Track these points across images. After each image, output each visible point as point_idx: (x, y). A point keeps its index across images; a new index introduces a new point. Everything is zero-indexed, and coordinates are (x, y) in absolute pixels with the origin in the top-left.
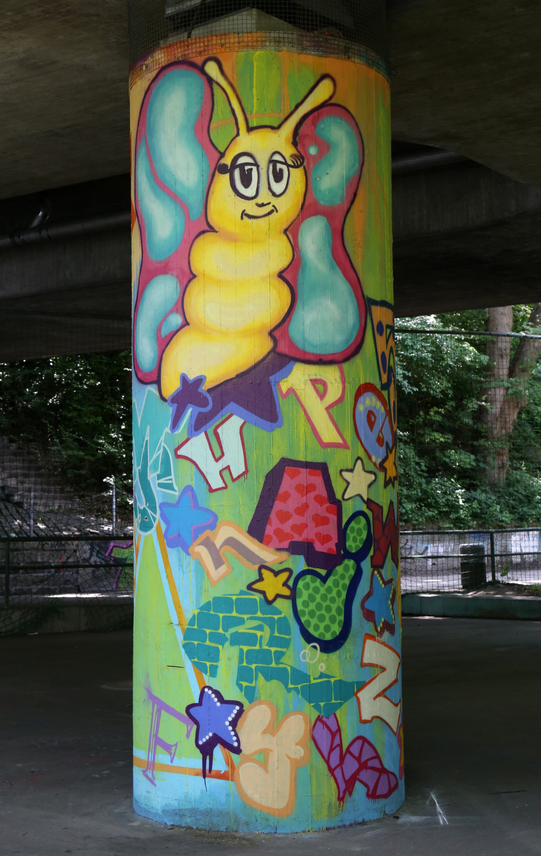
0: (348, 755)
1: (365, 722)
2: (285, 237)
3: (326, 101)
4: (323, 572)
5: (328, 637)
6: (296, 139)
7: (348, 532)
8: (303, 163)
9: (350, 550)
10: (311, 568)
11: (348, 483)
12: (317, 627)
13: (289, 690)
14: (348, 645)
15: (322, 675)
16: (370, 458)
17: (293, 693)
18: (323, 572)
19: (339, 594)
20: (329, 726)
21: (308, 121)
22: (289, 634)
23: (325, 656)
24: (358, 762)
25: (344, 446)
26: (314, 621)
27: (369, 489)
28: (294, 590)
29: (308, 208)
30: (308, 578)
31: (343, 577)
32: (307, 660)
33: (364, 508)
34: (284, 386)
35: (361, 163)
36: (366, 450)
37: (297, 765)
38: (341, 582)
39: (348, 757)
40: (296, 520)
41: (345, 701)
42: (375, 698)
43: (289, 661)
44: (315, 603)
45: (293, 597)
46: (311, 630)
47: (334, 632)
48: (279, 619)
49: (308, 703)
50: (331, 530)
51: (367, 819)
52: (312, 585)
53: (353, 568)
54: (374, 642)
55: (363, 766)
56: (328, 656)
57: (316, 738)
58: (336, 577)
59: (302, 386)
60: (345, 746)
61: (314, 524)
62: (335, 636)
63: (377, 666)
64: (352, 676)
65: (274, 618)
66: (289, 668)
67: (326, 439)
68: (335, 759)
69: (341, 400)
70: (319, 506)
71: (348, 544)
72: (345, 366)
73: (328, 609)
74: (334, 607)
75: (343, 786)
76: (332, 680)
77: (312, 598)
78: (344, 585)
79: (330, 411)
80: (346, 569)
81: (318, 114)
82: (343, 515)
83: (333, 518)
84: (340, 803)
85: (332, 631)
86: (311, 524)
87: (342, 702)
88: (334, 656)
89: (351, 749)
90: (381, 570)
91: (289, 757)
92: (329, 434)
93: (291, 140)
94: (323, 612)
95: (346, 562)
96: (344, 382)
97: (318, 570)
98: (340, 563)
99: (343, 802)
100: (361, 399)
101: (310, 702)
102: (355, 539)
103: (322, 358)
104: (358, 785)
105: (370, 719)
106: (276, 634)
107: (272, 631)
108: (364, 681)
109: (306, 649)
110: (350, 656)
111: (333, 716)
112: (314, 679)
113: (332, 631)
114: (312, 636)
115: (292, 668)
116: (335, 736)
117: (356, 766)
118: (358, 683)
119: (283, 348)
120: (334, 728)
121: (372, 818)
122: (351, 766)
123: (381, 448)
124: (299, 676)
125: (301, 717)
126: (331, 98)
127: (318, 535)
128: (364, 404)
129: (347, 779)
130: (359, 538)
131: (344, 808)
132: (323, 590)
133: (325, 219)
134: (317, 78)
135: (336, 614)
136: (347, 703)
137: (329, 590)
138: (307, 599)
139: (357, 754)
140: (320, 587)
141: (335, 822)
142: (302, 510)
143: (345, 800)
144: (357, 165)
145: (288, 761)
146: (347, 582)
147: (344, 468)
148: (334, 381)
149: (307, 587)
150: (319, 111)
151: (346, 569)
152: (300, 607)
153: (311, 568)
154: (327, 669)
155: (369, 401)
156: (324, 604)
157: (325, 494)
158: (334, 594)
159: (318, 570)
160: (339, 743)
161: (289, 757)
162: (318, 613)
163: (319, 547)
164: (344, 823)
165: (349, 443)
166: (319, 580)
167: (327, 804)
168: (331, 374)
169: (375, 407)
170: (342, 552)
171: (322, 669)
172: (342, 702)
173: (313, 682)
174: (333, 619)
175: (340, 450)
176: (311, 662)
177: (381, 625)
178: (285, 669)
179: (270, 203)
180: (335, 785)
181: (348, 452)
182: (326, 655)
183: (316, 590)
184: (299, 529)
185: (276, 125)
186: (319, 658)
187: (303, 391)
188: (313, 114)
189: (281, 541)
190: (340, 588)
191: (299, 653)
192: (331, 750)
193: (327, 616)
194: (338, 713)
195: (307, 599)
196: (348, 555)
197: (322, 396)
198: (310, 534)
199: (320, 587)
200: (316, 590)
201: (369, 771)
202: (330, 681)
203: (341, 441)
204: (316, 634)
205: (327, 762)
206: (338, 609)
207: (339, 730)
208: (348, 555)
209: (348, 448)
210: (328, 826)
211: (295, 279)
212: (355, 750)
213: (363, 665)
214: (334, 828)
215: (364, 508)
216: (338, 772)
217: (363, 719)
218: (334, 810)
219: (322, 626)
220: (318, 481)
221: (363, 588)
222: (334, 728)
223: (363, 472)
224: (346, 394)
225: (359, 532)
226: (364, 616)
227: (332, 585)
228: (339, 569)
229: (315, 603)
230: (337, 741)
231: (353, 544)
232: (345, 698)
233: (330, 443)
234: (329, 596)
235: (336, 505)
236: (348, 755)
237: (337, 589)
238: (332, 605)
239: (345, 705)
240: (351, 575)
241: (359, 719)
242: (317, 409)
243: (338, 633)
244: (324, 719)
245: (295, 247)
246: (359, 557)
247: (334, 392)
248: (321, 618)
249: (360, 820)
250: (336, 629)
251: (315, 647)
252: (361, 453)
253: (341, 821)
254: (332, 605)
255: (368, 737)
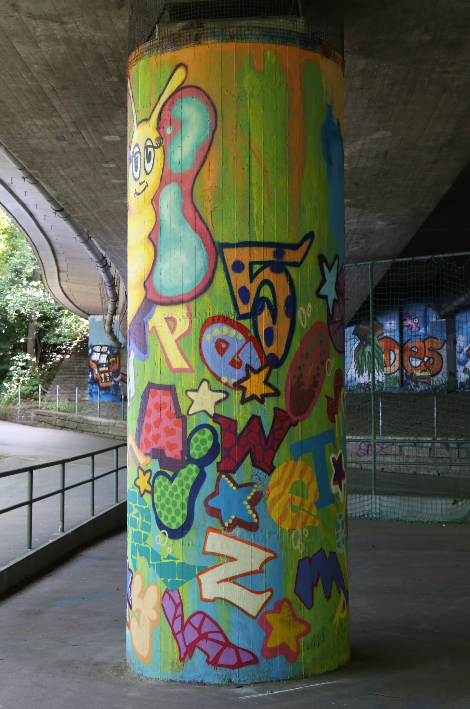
0: (189, 625)
1: (206, 600)
2: (151, 206)
3: (179, 87)
4: (171, 474)
5: (174, 526)
6: (159, 127)
7: (192, 441)
8: (161, 144)
9: (193, 457)
10: (162, 470)
11: (193, 401)
12: (166, 518)
13: (150, 565)
14: (191, 534)
15: (169, 557)
16: (219, 379)
17: (152, 567)
18: (171, 474)
19: (183, 492)
20: (174, 598)
21: (166, 108)
22: (150, 522)
23: (171, 541)
24: (198, 632)
25: (191, 370)
26: (164, 513)
27: (217, 406)
28: (152, 486)
29: (166, 179)
30: (161, 477)
31: (186, 478)
32: (160, 543)
33: (210, 422)
34: (150, 325)
35: (213, 128)
36: (212, 373)
37: (153, 624)
38: (185, 483)
39: (189, 627)
40: (154, 431)
41: (187, 580)
42: (218, 582)
43: (150, 543)
44: (165, 498)
45: (152, 493)
46: (162, 519)
47: (178, 523)
48: (146, 508)
49: (159, 578)
50: (177, 439)
51: (206, 681)
52: (163, 484)
53: (196, 471)
54: (219, 535)
55: (203, 636)
56: (173, 542)
57: (165, 606)
58: (181, 479)
59: (160, 325)
60: (186, 618)
61: (165, 435)
62: (179, 526)
63: (223, 555)
64: (194, 560)
65: (143, 508)
66: (150, 548)
67: (175, 366)
68: (177, 628)
69: (188, 332)
70: (169, 420)
71: (191, 451)
72: (192, 304)
73: (174, 504)
74: (179, 502)
75: (184, 650)
76: (177, 562)
77: (163, 494)
78: (187, 485)
79: (179, 342)
80: (190, 472)
81: (173, 99)
82: (188, 427)
83: (179, 430)
84: (181, 662)
85: (177, 522)
86: (163, 435)
87: (184, 580)
88: (179, 542)
89: (192, 621)
90: (232, 475)
91: (149, 618)
92: (178, 361)
93: (156, 127)
94: (170, 506)
95: (190, 466)
96: (190, 318)
97: (167, 472)
98: (183, 467)
99: (184, 662)
100: (208, 330)
101: (161, 577)
102: (198, 448)
103: (173, 299)
104: (197, 650)
105: (212, 599)
106: (144, 521)
107: (143, 519)
108: (206, 567)
109: (159, 534)
110: (192, 544)
111: (177, 591)
112: (164, 559)
113: (177, 522)
114: (163, 525)
115: (152, 549)
116: (178, 607)
117: (195, 635)
118: (199, 567)
119: (150, 296)
120: (177, 601)
121: (212, 682)
122: (191, 635)
123: (236, 370)
124: (155, 556)
125: (156, 587)
126: (183, 82)
127: (167, 443)
128: (211, 334)
129: (187, 644)
130: (202, 447)
131: (184, 667)
132: (170, 489)
133: (177, 185)
134: (173, 69)
135: (180, 509)
136: (189, 582)
137: (175, 489)
138: (160, 495)
139: (197, 626)
140: (168, 485)
141: (177, 677)
142: (158, 423)
143: (185, 661)
144: (208, 133)
145: (149, 621)
146: (190, 483)
147: (190, 388)
148: (181, 318)
149: (160, 484)
150: (173, 97)
151: (190, 472)
152: (156, 501)
153: (162, 470)
154: (173, 552)
155: (219, 331)
156: (171, 500)
157: (173, 411)
158: (179, 492)
159: (167, 472)
160: (181, 613)
161: (149, 618)
162: (167, 506)
163: (169, 454)
164: (184, 679)
165: (194, 368)
166: (168, 480)
167: (171, 661)
168: (179, 312)
169: (227, 335)
170: (186, 458)
171: (169, 551)
172: (184, 580)
173: (163, 561)
174: (177, 513)
175: (186, 374)
176: (162, 545)
177: (231, 521)
178: (148, 548)
179: (144, 181)
180: (177, 647)
181: (193, 376)
182: (172, 540)
183: (166, 488)
184: (156, 438)
185: (148, 117)
186: (167, 543)
187: (160, 328)
188: (169, 101)
189: (147, 448)
190: (184, 487)
191: (155, 537)
192: (175, 618)
193: (173, 509)
194: (180, 589)
195: (160, 495)
196: (191, 460)
197: (172, 331)
198: (162, 443)
199: (168, 485)
200: (166, 488)
201: (210, 642)
202: (175, 563)
203: (186, 366)
204: (165, 523)
205: (172, 627)
206: (182, 504)
207: (181, 603)
208: (191, 460)
209: (193, 372)
210: (172, 679)
211: (157, 238)
212: (196, 621)
213: (205, 553)
214: (176, 681)
215: (210, 422)
216: (179, 637)
217: (204, 597)
218: (176, 667)
219: (170, 517)
220: (168, 399)
221: (207, 488)
222: (177, 601)
223: (210, 392)
224: (192, 327)
225: (204, 442)
226: (207, 512)
227: (177, 485)
228: (183, 472)
229: (165, 498)
230: (179, 612)
231: (197, 451)
232: (188, 578)
233: (178, 369)
234: (175, 493)
235: (183, 420)
236: (188, 625)
237: (181, 488)
238: (177, 501)
239: (187, 584)
240: (194, 477)
241: (200, 597)
242: (169, 340)
243: (181, 524)
244: (170, 592)
245: (157, 213)
246: (202, 463)
247: (182, 326)
248: (169, 511)
249: (199, 680)
250: (180, 521)
251: (164, 533)
252: (207, 375)
253: (182, 677)
254: (177, 501)
255: (209, 613)
